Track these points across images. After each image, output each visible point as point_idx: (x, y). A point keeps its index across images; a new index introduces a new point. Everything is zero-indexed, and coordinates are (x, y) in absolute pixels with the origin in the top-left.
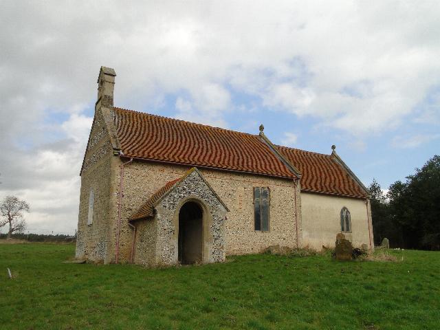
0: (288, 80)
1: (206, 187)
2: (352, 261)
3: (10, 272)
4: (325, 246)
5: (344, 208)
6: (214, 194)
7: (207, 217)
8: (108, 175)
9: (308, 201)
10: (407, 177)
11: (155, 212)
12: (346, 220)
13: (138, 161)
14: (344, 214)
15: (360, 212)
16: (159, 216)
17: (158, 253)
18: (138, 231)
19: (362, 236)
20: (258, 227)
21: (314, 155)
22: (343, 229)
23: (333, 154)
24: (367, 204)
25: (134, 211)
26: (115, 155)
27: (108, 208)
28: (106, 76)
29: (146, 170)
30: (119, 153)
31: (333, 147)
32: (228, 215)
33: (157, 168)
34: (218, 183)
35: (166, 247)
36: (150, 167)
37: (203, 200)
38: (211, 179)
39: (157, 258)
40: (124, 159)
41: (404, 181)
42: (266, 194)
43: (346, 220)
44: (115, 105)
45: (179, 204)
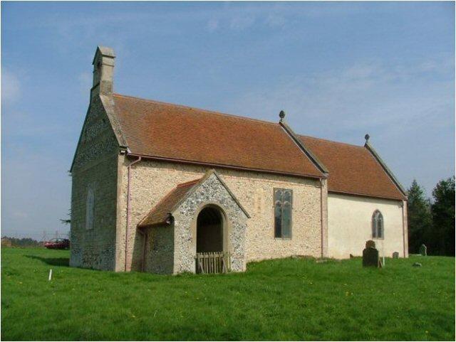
3: (50, 276)
5: (377, 211)
6: (234, 199)
9: (336, 204)
11: (171, 219)
12: (378, 226)
14: (376, 218)
15: (395, 216)
16: (176, 223)
18: (149, 238)
19: (394, 244)
20: (279, 232)
21: (339, 147)
22: (374, 236)
24: (402, 206)
29: (232, 259)
30: (127, 152)
32: (249, 222)
34: (235, 183)
35: (185, 255)
38: (232, 181)
42: (288, 196)
43: (378, 226)
45: (197, 210)
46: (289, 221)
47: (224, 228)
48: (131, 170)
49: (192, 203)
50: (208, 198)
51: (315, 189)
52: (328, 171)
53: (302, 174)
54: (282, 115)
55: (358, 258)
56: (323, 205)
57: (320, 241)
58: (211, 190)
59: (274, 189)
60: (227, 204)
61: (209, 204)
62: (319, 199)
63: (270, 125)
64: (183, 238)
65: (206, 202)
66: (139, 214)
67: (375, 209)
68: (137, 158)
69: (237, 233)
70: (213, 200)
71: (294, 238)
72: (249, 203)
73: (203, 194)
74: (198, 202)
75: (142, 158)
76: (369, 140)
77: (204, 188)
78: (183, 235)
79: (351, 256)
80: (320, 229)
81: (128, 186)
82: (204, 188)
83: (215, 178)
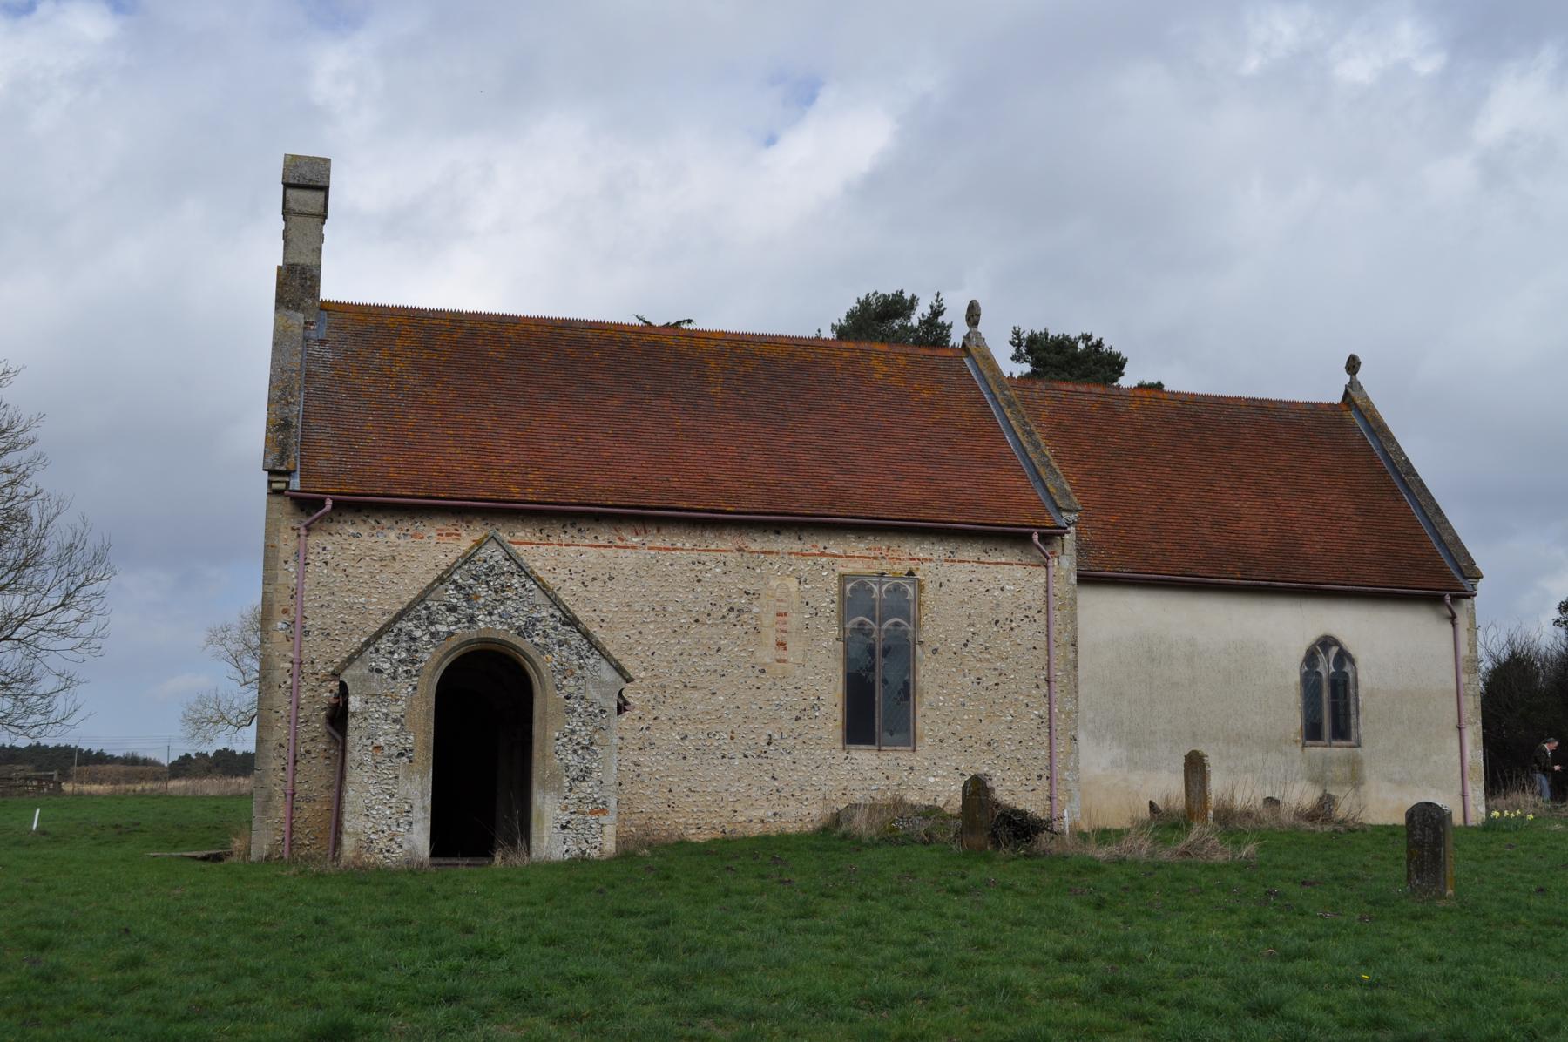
1: (538, 597)
4: (1160, 804)
6: (571, 621)
7: (546, 702)
14: (1326, 667)
27: (1030, 459)
29: (392, 536)
31: (1353, 365)
36: (406, 525)
37: (524, 644)
45: (432, 659)
46: (906, 684)
49: (414, 639)
50: (472, 620)
51: (1020, 572)
53: (955, 519)
55: (1401, 826)
58: (485, 594)
59: (844, 578)
60: (546, 636)
61: (480, 640)
64: (377, 748)
67: (1312, 636)
69: (583, 733)
70: (490, 625)
72: (737, 631)
73: (453, 609)
74: (434, 635)
75: (337, 505)
76: (1359, 376)
77: (459, 587)
78: (381, 741)
79: (977, 789)
82: (459, 587)
83: (499, 555)
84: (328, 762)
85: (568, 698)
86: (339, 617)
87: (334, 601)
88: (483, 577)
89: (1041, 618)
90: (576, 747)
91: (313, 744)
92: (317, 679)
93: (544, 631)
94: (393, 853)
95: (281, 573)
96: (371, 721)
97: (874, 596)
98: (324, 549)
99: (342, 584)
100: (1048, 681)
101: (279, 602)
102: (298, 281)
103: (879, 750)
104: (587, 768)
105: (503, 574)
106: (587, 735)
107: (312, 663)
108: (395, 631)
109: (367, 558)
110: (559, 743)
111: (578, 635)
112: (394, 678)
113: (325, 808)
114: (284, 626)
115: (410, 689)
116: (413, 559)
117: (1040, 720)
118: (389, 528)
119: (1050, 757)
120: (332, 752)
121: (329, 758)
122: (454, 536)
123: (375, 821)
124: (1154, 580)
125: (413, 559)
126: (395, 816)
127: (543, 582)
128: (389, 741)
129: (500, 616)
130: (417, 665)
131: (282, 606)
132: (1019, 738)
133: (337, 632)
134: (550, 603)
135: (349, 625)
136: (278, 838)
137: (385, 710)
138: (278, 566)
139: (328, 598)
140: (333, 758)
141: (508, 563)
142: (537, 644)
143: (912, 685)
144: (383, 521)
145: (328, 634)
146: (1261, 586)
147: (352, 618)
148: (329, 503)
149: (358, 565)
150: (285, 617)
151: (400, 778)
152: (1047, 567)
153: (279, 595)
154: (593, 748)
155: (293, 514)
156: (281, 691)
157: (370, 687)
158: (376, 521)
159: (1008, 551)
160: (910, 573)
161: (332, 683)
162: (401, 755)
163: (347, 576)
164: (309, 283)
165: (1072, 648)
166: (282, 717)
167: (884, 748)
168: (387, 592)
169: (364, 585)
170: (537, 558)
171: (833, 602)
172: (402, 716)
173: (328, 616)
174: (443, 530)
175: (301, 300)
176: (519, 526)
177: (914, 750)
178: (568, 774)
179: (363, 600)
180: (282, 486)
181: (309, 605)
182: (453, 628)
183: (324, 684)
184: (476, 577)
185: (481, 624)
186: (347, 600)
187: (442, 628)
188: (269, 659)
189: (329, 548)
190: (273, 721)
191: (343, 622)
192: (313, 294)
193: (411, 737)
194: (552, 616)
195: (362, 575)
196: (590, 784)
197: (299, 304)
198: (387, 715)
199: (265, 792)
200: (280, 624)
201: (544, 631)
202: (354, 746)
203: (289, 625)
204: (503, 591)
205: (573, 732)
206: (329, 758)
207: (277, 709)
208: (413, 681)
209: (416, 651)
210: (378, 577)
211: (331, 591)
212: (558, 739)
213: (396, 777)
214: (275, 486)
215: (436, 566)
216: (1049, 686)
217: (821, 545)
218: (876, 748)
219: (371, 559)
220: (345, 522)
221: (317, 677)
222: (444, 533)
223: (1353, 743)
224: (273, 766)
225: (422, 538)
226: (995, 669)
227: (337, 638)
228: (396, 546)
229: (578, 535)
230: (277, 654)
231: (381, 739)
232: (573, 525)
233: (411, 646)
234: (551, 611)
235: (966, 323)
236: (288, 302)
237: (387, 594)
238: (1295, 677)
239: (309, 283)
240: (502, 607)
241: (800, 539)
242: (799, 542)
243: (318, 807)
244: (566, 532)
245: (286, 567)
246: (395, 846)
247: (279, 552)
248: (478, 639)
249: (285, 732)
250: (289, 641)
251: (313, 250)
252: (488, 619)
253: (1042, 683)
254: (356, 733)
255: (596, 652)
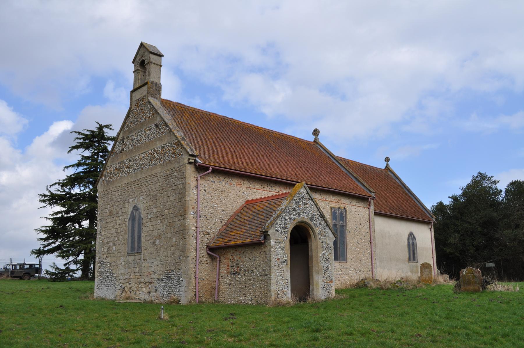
0: (259, 70)
1: (315, 208)
2: (482, 292)
5: (411, 234)
8: (182, 193)
10: (450, 197)
11: (266, 235)
13: (218, 172)
16: (272, 242)
17: (274, 288)
23: (387, 168)
25: (212, 235)
26: (190, 163)
28: (152, 56)
29: (224, 183)
33: (234, 181)
36: (227, 179)
37: (311, 223)
39: (273, 294)
40: (201, 169)
41: (447, 202)
44: (163, 97)
46: (344, 242)
47: (313, 248)
48: (201, 182)
49: (286, 220)
50: (299, 214)
52: (374, 191)
54: (387, 160)
56: (371, 226)
57: (370, 263)
58: (302, 206)
59: (331, 208)
62: (368, 220)
63: (307, 143)
65: (298, 219)
66: (209, 234)
68: (207, 169)
70: (304, 217)
71: (349, 260)
73: (295, 210)
74: (290, 218)
75: (213, 169)
78: (279, 257)
80: (370, 251)
81: (197, 202)
82: (296, 203)
84: (207, 265)
85: (322, 243)
86: (209, 211)
87: (208, 205)
88: (301, 199)
89: (368, 223)
90: (325, 260)
91: (203, 258)
92: (203, 234)
93: (316, 220)
94: (284, 298)
95: (191, 193)
96: (277, 249)
97: (344, 215)
98: (205, 186)
99: (210, 199)
100: (370, 242)
101: (191, 204)
102: (155, 88)
103: (340, 262)
104: (328, 267)
105: (306, 199)
106: (327, 256)
107: (202, 228)
108: (281, 217)
109: (217, 190)
110: (321, 258)
111: (323, 221)
112: (281, 234)
113: (207, 283)
114: (193, 213)
115: (285, 238)
116: (230, 192)
117: (369, 254)
118: (222, 180)
119: (372, 265)
120: (208, 261)
121: (207, 264)
122: (240, 185)
123: (279, 286)
124: (385, 214)
125: (230, 192)
126: (284, 285)
127: (317, 203)
128: (281, 257)
129: (306, 213)
130: (287, 230)
131: (192, 206)
132: (366, 259)
133: (209, 217)
134: (317, 210)
135: (212, 214)
136: (193, 294)
137: (280, 246)
138: (191, 191)
139: (206, 204)
140: (209, 264)
141: (307, 195)
142: (314, 224)
143: (345, 242)
144: (221, 177)
145: (207, 217)
146: (403, 217)
147: (213, 212)
148: (211, 169)
149: (215, 193)
150: (193, 210)
151: (285, 270)
152: (369, 209)
153: (191, 201)
154: (329, 260)
155: (194, 172)
156: (193, 238)
157: (276, 237)
158: (219, 177)
159: (361, 203)
160: (344, 208)
161: (208, 235)
162: (284, 262)
163: (212, 196)
164: (158, 89)
165: (374, 233)
166: (193, 248)
167: (341, 262)
168: (223, 203)
169: (216, 200)
170: (262, 195)
171: (329, 215)
172: (284, 248)
173: (207, 211)
174: (237, 182)
175: (156, 94)
176: (256, 183)
177: (347, 262)
178: (324, 269)
179: (216, 205)
180: (193, 161)
181: (201, 206)
182: (295, 216)
183: (205, 236)
184: (300, 199)
185: (301, 216)
186: (212, 205)
187: (292, 216)
188: (189, 226)
189: (206, 185)
190: (191, 249)
191: (211, 213)
192: (160, 93)
193: (287, 256)
194: (318, 214)
195: (216, 196)
196: (329, 272)
197: (155, 96)
198: (280, 247)
199: (188, 276)
200: (191, 212)
201: (316, 220)
202: (273, 259)
203: (194, 213)
204: (306, 205)
205: (324, 254)
206: (207, 264)
207: (192, 245)
208: (286, 235)
209: (286, 224)
210: (220, 197)
211: (207, 202)
212: (321, 257)
213: (284, 270)
214: (191, 160)
215: (237, 195)
216: (371, 244)
217: (325, 197)
218: (339, 262)
219: (219, 191)
220: (210, 176)
221: (203, 233)
222: (238, 184)
223: (416, 262)
224: (191, 267)
225: (232, 185)
226: (361, 238)
227: (209, 219)
228: (225, 187)
229: (271, 188)
230: (191, 224)
231: (279, 256)
232: (269, 184)
233: (285, 222)
234: (317, 213)
235: (320, 132)
236: (152, 94)
237: (223, 204)
238: (406, 243)
239: (158, 89)
240: (306, 210)
241: (321, 195)
242: (320, 196)
243: (205, 282)
244: (268, 187)
245: (193, 191)
246: (284, 295)
247: (190, 185)
248: (301, 221)
249: (194, 253)
250: (194, 219)
251: (158, 77)
252: (303, 214)
253: (369, 243)
254: (273, 254)
255: (328, 227)
